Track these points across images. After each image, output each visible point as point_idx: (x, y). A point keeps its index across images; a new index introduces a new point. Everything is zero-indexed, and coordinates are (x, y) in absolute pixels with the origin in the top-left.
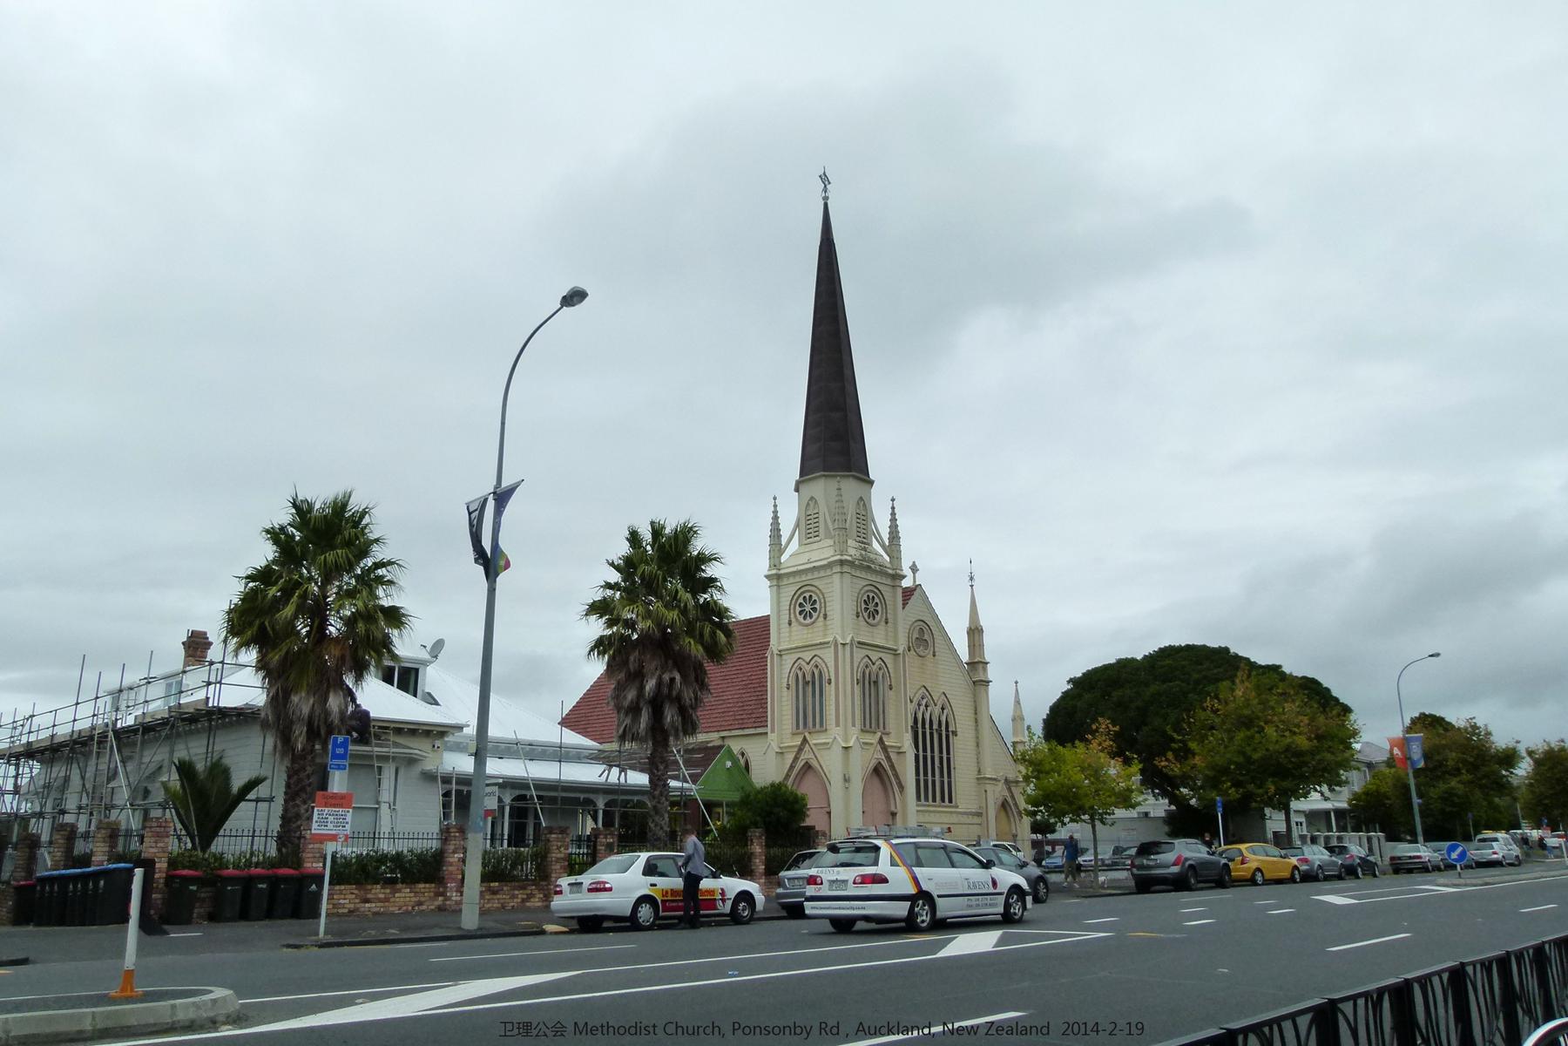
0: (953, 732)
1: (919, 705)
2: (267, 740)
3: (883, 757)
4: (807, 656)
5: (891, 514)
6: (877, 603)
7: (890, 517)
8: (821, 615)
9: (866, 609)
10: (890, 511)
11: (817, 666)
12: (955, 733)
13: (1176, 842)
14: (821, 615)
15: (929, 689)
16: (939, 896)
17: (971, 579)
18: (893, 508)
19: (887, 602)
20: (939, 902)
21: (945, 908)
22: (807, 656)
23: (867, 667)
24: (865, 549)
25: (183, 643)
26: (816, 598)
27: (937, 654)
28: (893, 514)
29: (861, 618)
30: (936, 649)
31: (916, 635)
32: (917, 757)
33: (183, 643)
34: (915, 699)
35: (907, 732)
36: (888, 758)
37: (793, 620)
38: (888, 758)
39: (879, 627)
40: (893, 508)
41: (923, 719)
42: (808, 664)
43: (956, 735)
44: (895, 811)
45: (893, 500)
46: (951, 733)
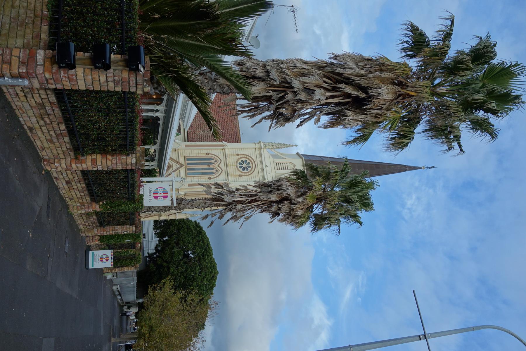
4: (222, 165)
37: (239, 157)
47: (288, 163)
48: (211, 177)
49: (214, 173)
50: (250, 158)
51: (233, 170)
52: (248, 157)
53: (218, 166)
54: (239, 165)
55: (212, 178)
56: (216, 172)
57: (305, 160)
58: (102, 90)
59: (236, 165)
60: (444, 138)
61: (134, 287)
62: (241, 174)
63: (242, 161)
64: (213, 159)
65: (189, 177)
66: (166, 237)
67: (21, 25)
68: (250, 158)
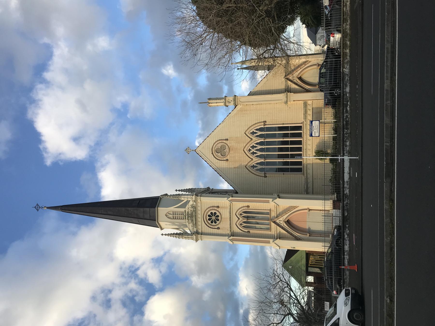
0: (265, 125)
4: (235, 219)
7: (169, 237)
14: (217, 209)
15: (245, 145)
18: (166, 235)
22: (235, 219)
30: (224, 139)
35: (268, 202)
37: (218, 226)
40: (166, 235)
41: (261, 150)
45: (162, 235)
47: (172, 217)
48: (246, 208)
49: (244, 212)
50: (208, 224)
51: (225, 214)
52: (210, 226)
53: (239, 219)
54: (219, 218)
55: (245, 206)
56: (251, 149)
57: (156, 221)
58: (323, 201)
59: (221, 218)
60: (224, 52)
61: (335, 154)
62: (217, 209)
63: (215, 223)
64: (244, 227)
65: (268, 210)
66: (314, 295)
67: (265, 5)
68: (208, 224)
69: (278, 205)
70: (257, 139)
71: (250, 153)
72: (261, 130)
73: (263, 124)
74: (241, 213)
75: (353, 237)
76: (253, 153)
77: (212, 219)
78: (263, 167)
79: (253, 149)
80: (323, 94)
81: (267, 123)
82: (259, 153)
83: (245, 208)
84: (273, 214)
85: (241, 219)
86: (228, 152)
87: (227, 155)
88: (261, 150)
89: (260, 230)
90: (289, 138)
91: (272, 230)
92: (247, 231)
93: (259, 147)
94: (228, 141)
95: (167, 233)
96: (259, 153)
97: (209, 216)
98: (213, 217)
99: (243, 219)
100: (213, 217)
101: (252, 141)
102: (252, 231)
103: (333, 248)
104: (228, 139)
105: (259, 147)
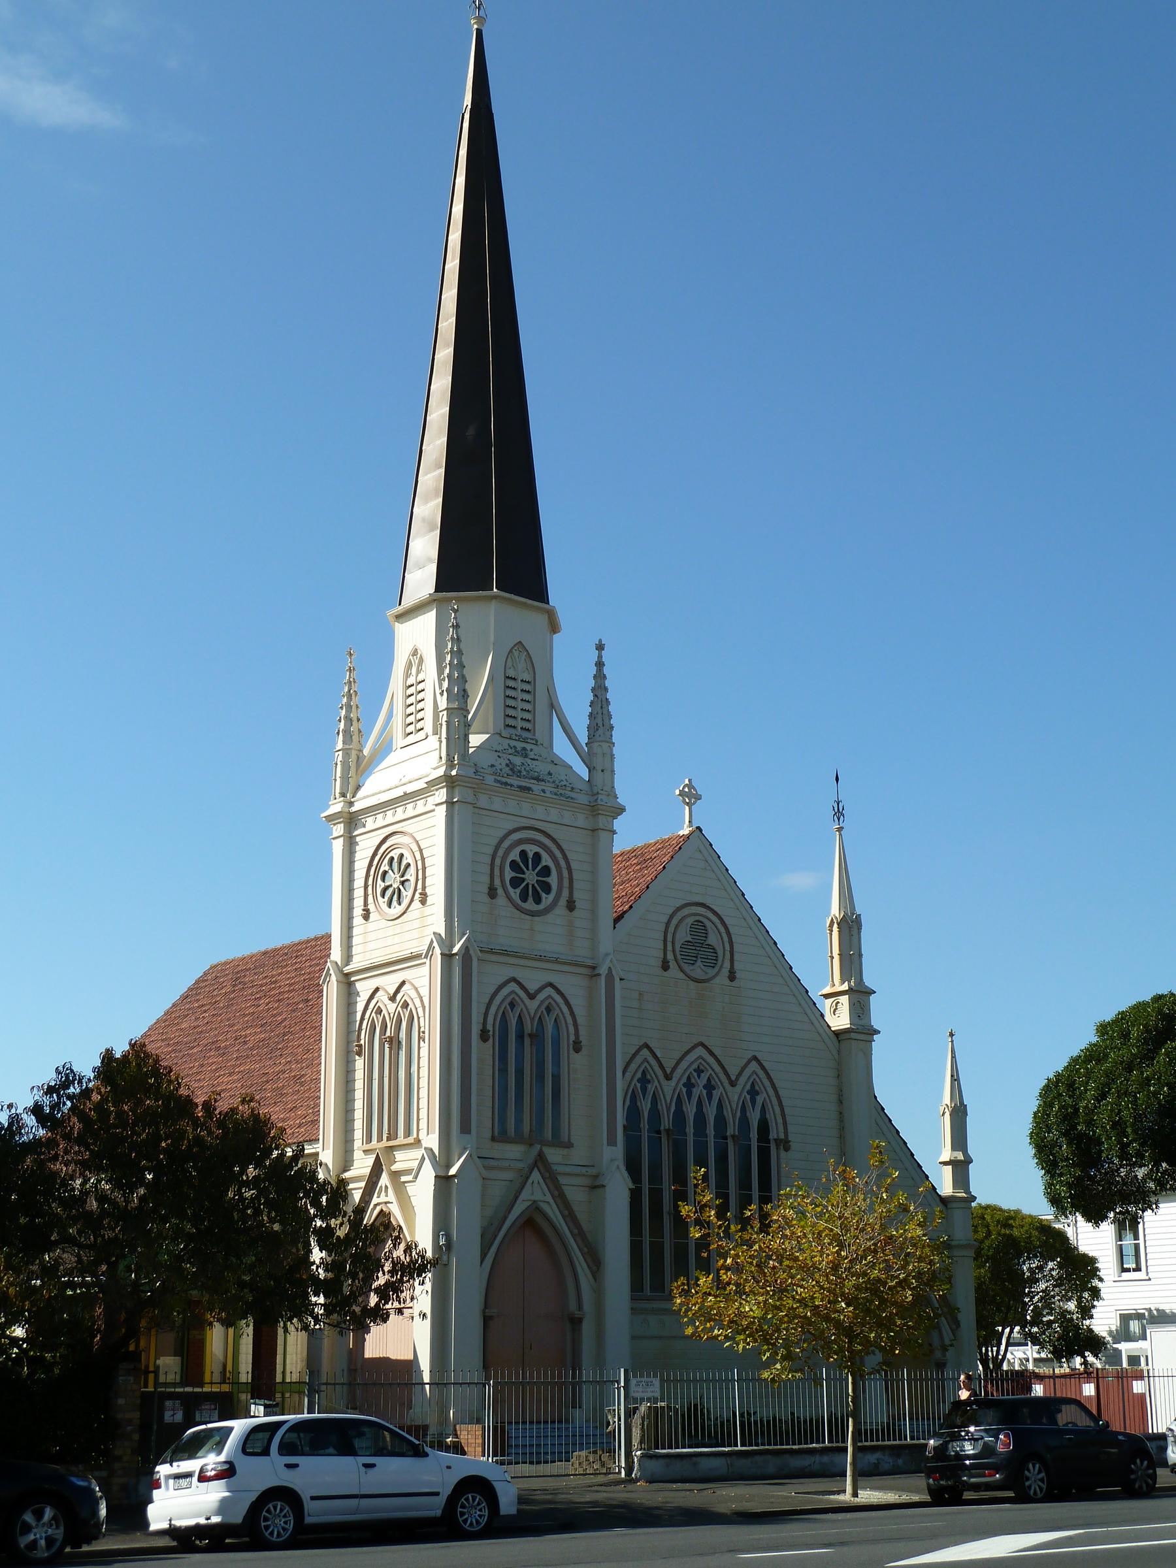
0: (778, 1141)
1: (689, 1085)
2: (507, 1182)
3: (549, 1198)
5: (595, 677)
6: (383, 880)
8: (417, 896)
9: (515, 882)
10: (594, 670)
11: (405, 1005)
12: (785, 1144)
13: (1104, 1334)
14: (563, 902)
15: (717, 1052)
16: (313, 1498)
17: (839, 814)
18: (600, 664)
19: (574, 865)
20: (309, 1506)
21: (315, 1513)
23: (512, 1005)
24: (524, 753)
25: (621, 810)
26: (536, 849)
27: (737, 975)
28: (600, 676)
29: (501, 900)
30: (737, 966)
31: (683, 935)
32: (635, 1195)
33: (621, 810)
34: (679, 1071)
35: (612, 1142)
36: (560, 1197)
38: (560, 1197)
39: (549, 917)
40: (600, 664)
41: (700, 1117)
42: (532, 997)
43: (787, 1149)
44: (577, 1314)
46: (773, 1146)
69: (416, 1177)
70: (734, 1107)
71: (710, 1071)
72: (764, 1127)
73: (782, 1136)
74: (411, 1006)
75: (774, 1555)
76: (689, 1085)
77: (536, 871)
78: (690, 1130)
79: (705, 1087)
80: (178, 1359)
81: (783, 1154)
82: (690, 1110)
83: (572, 1029)
84: (554, 1155)
85: (533, 1005)
86: (689, 972)
87: (682, 970)
88: (700, 1117)
89: (662, 1095)
90: (643, 1239)
91: (496, 1145)
92: (489, 1027)
93: (711, 1112)
94: (727, 982)
95: (606, 670)
96: (690, 1110)
97: (514, 865)
98: (536, 878)
99: (532, 1014)
100: (536, 878)
101: (727, 1084)
102: (387, 1046)
103: (434, 1439)
104: (733, 984)
105: (711, 1112)
